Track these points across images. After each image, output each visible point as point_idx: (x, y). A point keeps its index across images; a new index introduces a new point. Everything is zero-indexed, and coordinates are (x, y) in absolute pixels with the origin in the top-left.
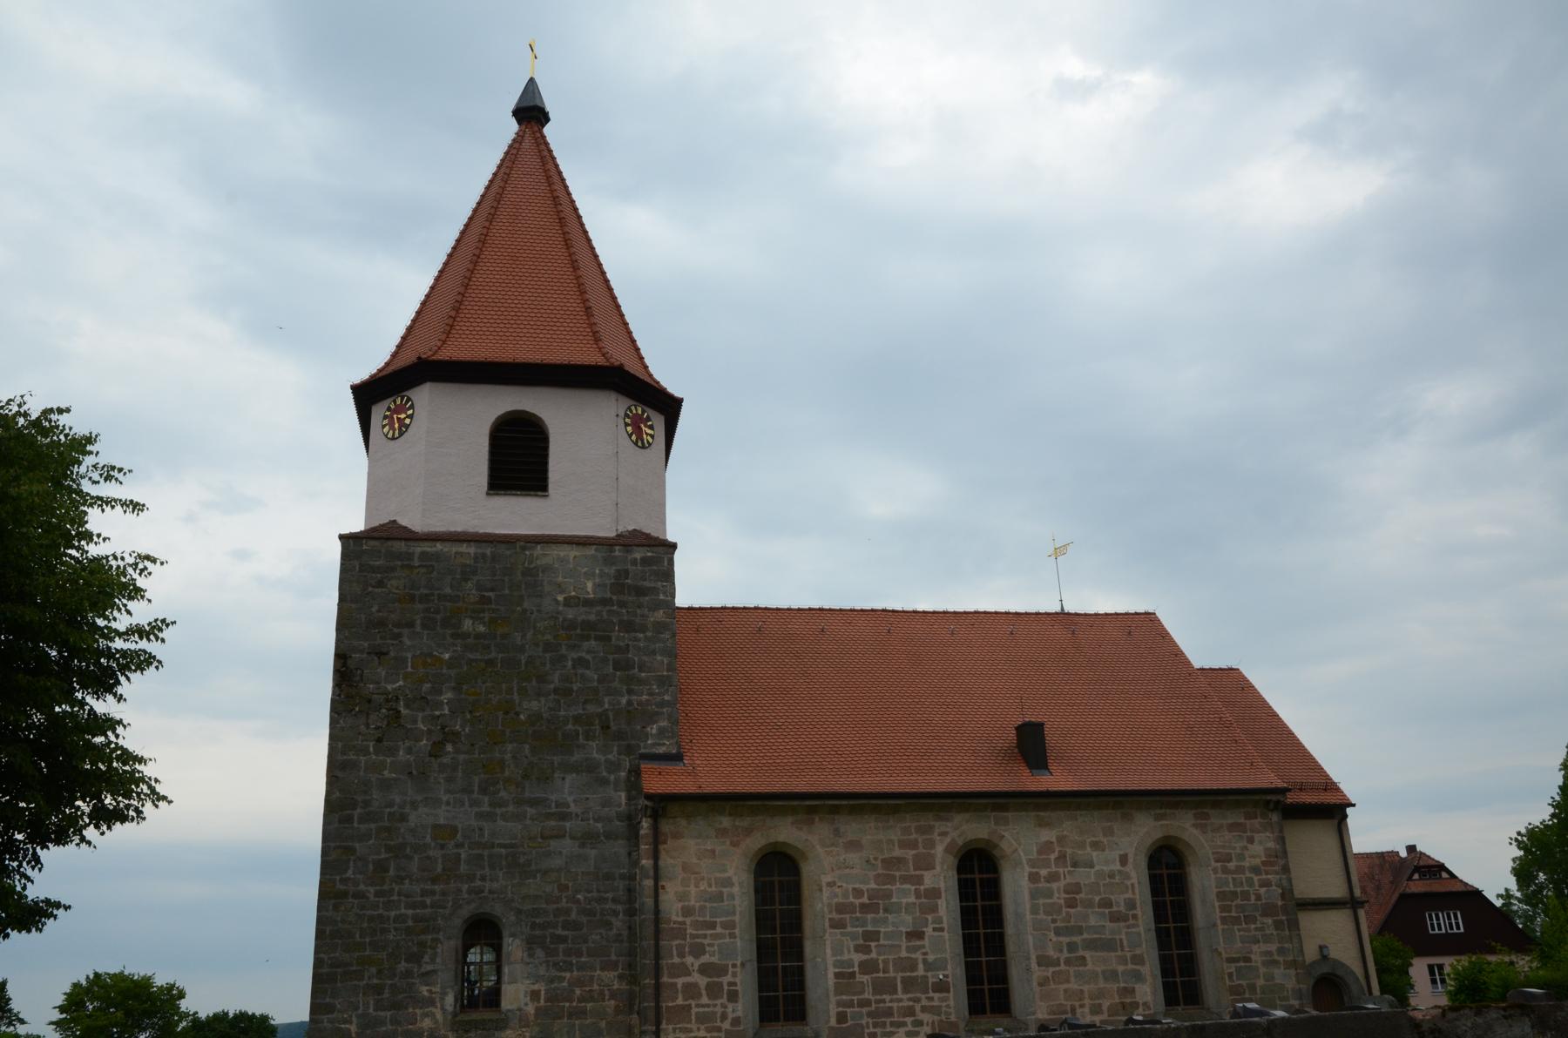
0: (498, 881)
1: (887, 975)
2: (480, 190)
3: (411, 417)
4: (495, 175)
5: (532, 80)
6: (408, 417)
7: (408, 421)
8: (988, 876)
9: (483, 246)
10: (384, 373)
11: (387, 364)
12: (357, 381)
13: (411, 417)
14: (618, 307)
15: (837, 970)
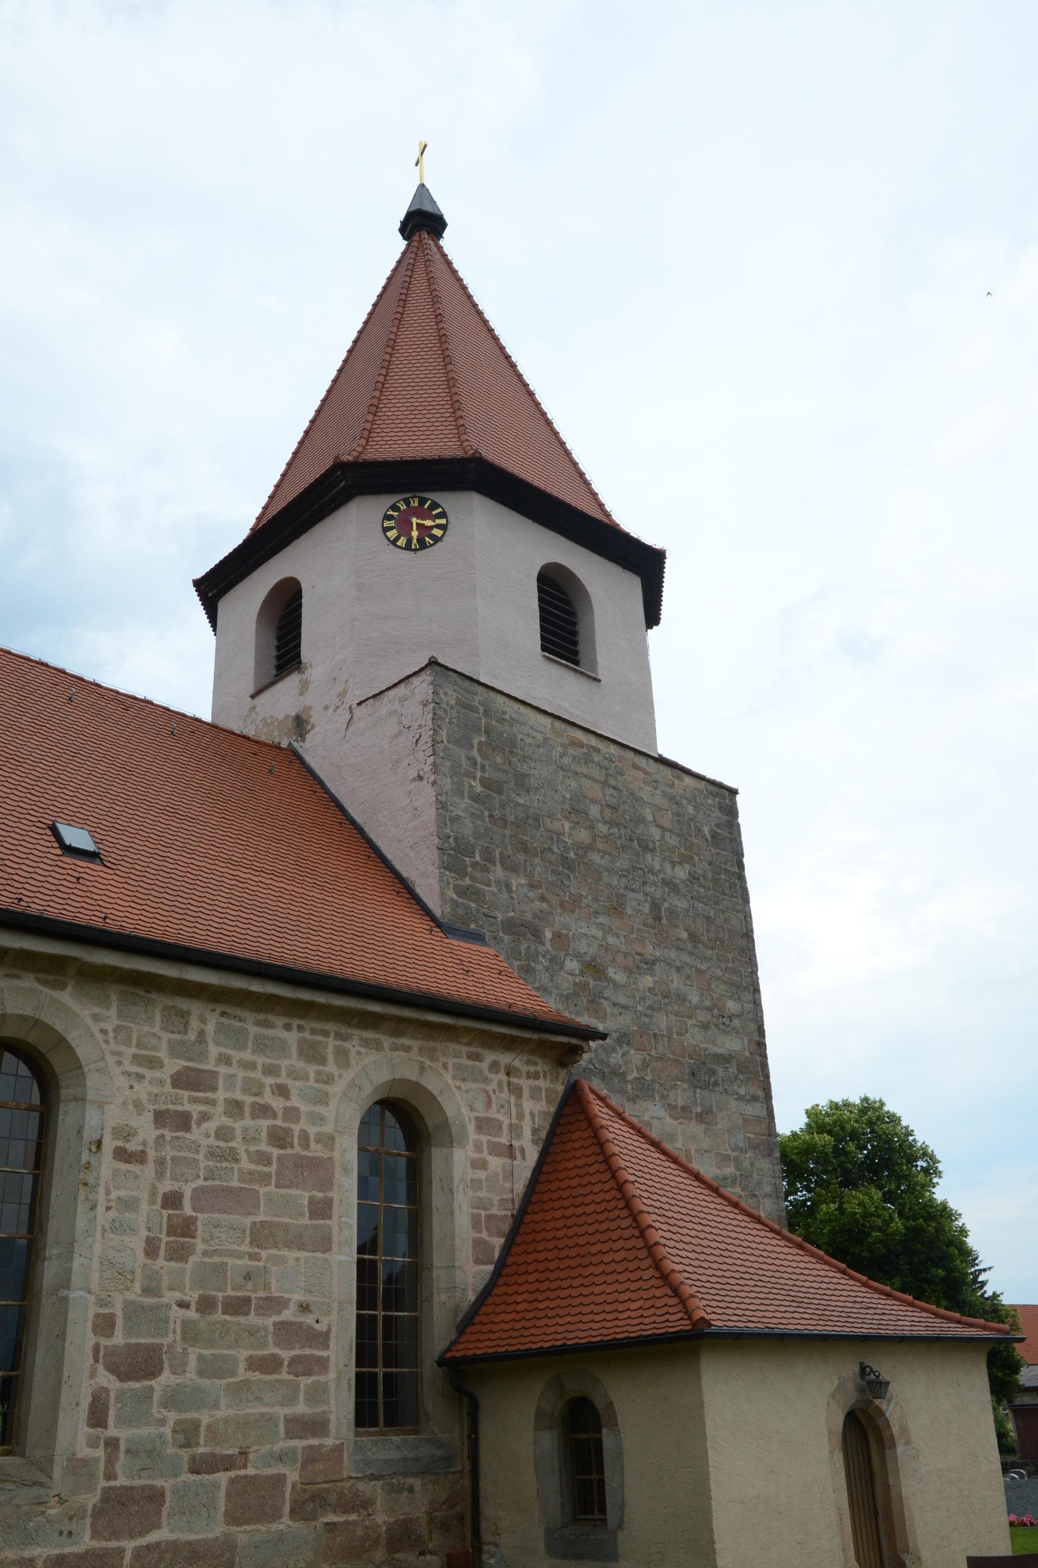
0: (292, 1147)
1: (112, 1483)
2: (523, 475)
3: (443, 527)
4: (399, 262)
5: (422, 186)
6: (439, 526)
7: (438, 532)
8: (397, 1370)
9: (400, 324)
10: (264, 521)
11: (265, 508)
12: (200, 573)
13: (443, 527)
14: (464, 288)
15: (327, 1222)
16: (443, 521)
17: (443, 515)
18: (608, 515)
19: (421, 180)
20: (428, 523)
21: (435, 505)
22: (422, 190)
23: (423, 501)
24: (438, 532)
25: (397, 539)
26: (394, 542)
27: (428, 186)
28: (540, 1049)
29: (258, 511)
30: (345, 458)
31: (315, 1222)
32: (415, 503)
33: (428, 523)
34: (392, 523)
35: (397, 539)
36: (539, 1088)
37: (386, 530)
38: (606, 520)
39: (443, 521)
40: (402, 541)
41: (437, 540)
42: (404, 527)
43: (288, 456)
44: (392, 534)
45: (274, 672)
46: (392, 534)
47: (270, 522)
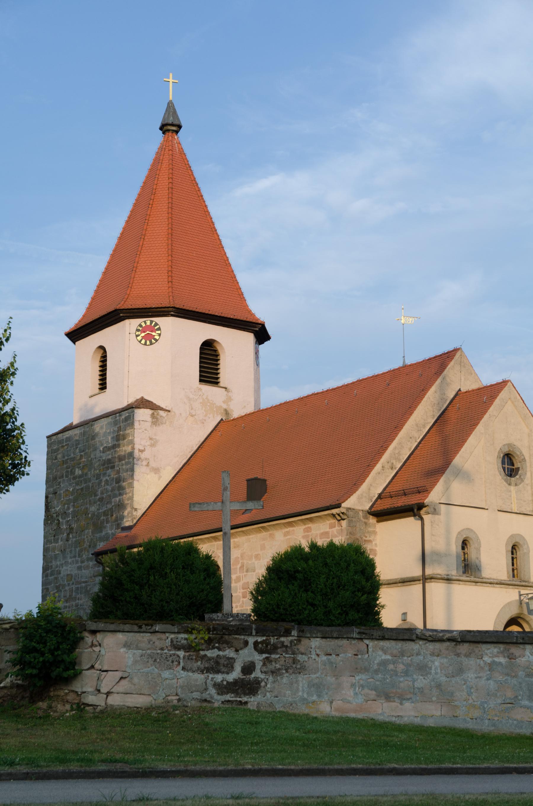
13: (160, 335)
17: (159, 329)
26: (140, 342)
32: (148, 323)
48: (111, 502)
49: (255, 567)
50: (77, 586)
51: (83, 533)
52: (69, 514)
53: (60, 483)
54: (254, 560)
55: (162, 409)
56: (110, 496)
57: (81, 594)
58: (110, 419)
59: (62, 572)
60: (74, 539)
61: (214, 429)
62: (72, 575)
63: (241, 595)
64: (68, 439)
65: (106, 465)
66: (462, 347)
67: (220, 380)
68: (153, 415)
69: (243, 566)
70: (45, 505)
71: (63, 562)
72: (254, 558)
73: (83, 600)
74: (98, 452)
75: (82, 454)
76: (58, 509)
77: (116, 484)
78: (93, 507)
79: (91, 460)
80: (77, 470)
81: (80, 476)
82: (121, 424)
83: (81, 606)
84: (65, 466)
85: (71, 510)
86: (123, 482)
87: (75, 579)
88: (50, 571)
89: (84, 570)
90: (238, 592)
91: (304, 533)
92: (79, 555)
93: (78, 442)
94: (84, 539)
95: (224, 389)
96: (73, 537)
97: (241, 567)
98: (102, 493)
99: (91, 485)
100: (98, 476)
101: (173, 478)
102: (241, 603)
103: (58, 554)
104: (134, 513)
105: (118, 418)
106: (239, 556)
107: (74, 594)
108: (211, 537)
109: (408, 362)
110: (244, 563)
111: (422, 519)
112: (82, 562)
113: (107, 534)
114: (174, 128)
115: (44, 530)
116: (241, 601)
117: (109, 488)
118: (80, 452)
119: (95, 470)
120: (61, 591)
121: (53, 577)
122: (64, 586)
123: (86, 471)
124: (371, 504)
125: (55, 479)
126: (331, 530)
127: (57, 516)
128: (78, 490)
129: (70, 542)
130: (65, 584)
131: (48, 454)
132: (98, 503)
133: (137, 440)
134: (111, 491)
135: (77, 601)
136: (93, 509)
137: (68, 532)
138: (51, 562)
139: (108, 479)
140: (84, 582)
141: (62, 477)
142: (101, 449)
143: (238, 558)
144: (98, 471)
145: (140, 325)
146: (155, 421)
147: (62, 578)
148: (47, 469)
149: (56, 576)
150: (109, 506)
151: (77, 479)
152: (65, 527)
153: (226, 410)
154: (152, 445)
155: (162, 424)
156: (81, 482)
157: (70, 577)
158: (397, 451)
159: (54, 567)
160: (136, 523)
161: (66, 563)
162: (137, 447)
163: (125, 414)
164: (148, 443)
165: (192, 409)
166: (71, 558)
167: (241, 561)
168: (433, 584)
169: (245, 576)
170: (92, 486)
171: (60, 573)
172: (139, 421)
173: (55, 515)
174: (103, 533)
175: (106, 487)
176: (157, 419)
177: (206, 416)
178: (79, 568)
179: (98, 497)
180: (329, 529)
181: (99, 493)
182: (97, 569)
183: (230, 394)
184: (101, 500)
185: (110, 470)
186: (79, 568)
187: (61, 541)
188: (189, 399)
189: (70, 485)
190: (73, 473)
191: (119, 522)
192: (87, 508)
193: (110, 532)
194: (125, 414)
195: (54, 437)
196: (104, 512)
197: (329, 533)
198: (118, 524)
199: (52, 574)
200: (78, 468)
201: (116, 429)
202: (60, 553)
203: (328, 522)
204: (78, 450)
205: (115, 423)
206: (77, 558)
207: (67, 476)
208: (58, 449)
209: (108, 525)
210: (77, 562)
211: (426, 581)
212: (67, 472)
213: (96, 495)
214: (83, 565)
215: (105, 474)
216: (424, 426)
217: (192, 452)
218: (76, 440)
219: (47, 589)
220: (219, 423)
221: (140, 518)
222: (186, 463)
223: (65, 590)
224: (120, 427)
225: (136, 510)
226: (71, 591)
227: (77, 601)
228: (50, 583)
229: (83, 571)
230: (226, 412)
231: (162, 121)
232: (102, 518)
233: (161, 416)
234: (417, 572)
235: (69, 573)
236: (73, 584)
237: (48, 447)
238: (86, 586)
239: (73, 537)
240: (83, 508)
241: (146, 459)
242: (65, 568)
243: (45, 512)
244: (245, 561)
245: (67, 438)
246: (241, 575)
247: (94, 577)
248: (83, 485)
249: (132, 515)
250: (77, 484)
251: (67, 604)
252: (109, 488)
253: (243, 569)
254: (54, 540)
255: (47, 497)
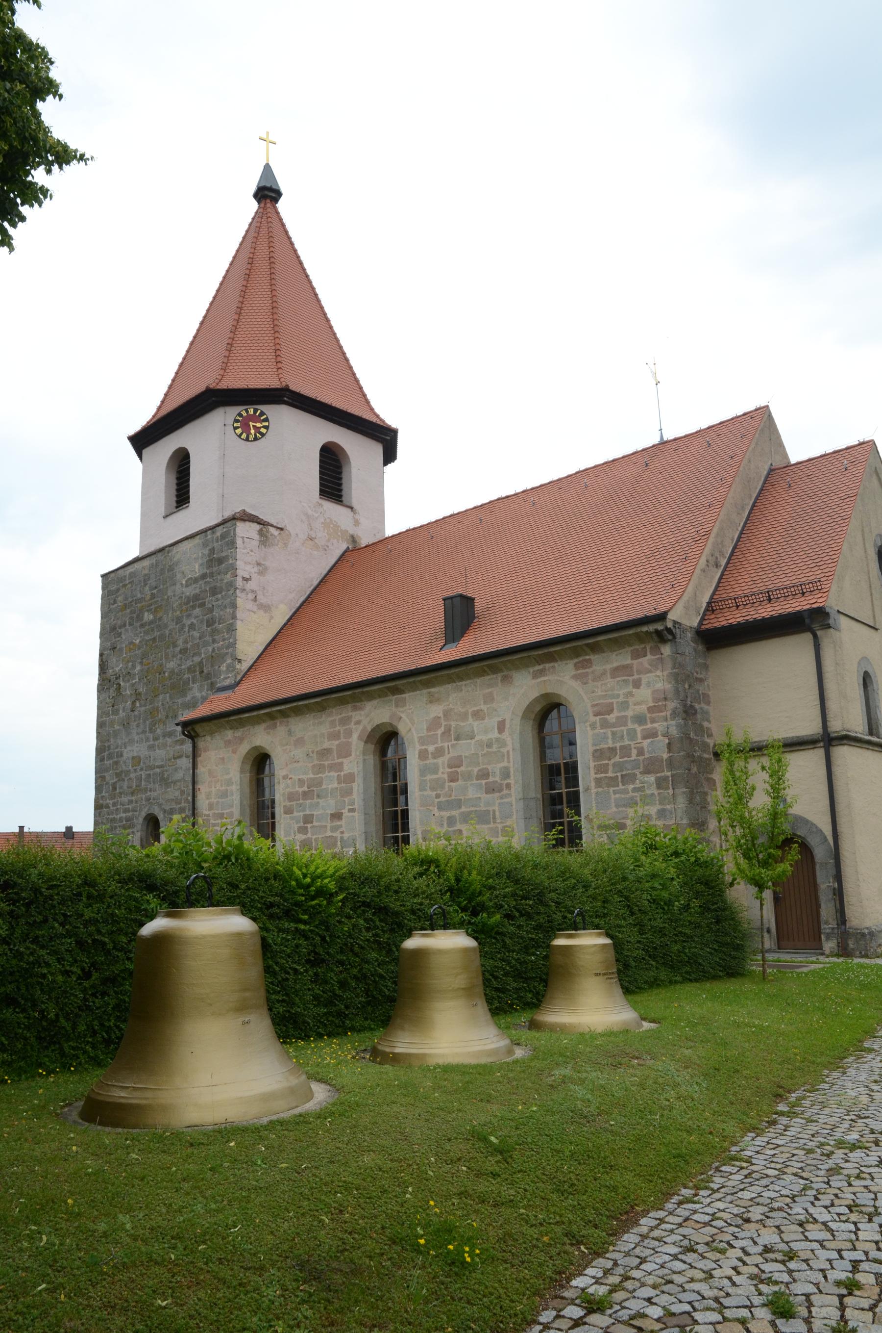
3: (267, 427)
6: (264, 427)
7: (263, 430)
11: (154, 416)
13: (267, 427)
16: (266, 424)
17: (267, 420)
18: (383, 421)
19: (268, 160)
20: (258, 425)
21: (262, 414)
22: (267, 169)
23: (256, 410)
24: (263, 430)
25: (242, 434)
26: (240, 436)
27: (271, 165)
28: (641, 638)
29: (151, 417)
30: (211, 387)
31: (579, 672)
32: (251, 411)
33: (258, 425)
34: (238, 425)
35: (242, 434)
36: (637, 650)
37: (235, 428)
38: (379, 422)
39: (266, 424)
40: (244, 436)
41: (263, 435)
42: (246, 427)
43: (362, 383)
44: (239, 431)
45: (175, 504)
46: (239, 431)
47: (154, 423)
48: (200, 654)
49: (473, 732)
50: (148, 772)
51: (156, 699)
52: (135, 675)
53: (121, 633)
54: (470, 719)
55: (272, 526)
56: (198, 645)
57: (154, 783)
58: (197, 540)
59: (125, 755)
60: (143, 708)
61: (339, 560)
62: (139, 758)
63: (446, 776)
64: (132, 575)
65: (191, 604)
66: (770, 404)
67: (344, 499)
68: (260, 532)
69: (450, 730)
70: (100, 665)
71: (127, 740)
72: (470, 717)
73: (158, 792)
74: (178, 586)
75: (155, 591)
76: (117, 669)
77: (207, 626)
78: (172, 663)
79: (168, 598)
80: (146, 614)
81: (151, 622)
82: (215, 545)
83: (154, 799)
84: (128, 611)
85: (138, 668)
86: (219, 624)
87: (144, 763)
88: (107, 753)
89: (159, 749)
90: (440, 773)
91: (577, 670)
92: (151, 729)
93: (147, 578)
94: (158, 707)
95: (349, 510)
96: (141, 706)
97: (443, 733)
98: (186, 642)
99: (167, 632)
100: (179, 620)
101: (289, 620)
102: (447, 789)
103: (119, 730)
104: (238, 667)
105: (209, 537)
106: (441, 715)
107: (143, 783)
108: (387, 688)
109: (668, 436)
110: (450, 726)
111: (815, 637)
112: (155, 739)
113: (194, 697)
114: (273, 195)
115: (98, 698)
116: (446, 787)
117: (196, 634)
118: (151, 589)
119: (174, 611)
120: (124, 780)
121: (111, 761)
122: (128, 772)
123: (159, 616)
124: (699, 618)
125: (113, 629)
126: (635, 662)
127: (117, 679)
128: (147, 641)
129: (136, 713)
130: (129, 771)
131: (102, 598)
132: (180, 656)
133: (240, 564)
134: (200, 638)
135: (149, 793)
136: (171, 665)
137: (133, 699)
138: (108, 740)
139: (195, 621)
140: (158, 767)
141: (125, 625)
142: (184, 582)
143: (439, 718)
144: (178, 613)
145: (240, 415)
146: (264, 539)
147: (125, 762)
148: (102, 618)
149: (115, 760)
150: (197, 659)
151: (147, 627)
152: (128, 692)
153: (352, 537)
154: (261, 573)
155: (273, 545)
156: (153, 630)
157: (137, 760)
158: (719, 540)
159: (112, 747)
160: (241, 680)
161: (131, 741)
162: (241, 573)
163: (219, 531)
164: (256, 569)
165: (311, 529)
166: (138, 734)
167: (444, 723)
168: (845, 748)
169: (453, 746)
170: (170, 634)
171: (122, 756)
172: (243, 538)
173: (113, 678)
174: (188, 698)
175: (191, 633)
176: (267, 537)
177: (328, 540)
178: (151, 748)
179: (178, 649)
180: (632, 659)
181: (180, 642)
182: (178, 747)
183: (357, 517)
184: (184, 651)
185: (198, 609)
186: (151, 748)
187: (124, 711)
188: (308, 517)
189: (136, 635)
190: (139, 618)
191: (213, 680)
192: (161, 665)
193: (198, 695)
194: (219, 531)
195: (113, 575)
196: (189, 669)
197: (631, 667)
198: (212, 683)
199: (110, 757)
200: (148, 611)
201: (206, 552)
202: (121, 728)
203: (531, 670)
204: (147, 588)
205: (205, 545)
206: (148, 734)
207: (130, 624)
208: (118, 590)
209: (195, 685)
210: (147, 740)
211: (834, 743)
212: (131, 618)
213: (175, 646)
214: (156, 743)
215: (189, 616)
216: (743, 508)
217: (312, 588)
218: (146, 575)
219: (103, 778)
220: (345, 552)
221: (246, 673)
222: (304, 602)
223: (130, 779)
224: (213, 548)
225: (240, 661)
226: (139, 779)
227: (149, 793)
228: (107, 770)
229: (157, 751)
230: (353, 540)
231: (259, 183)
232: (186, 676)
233: (272, 535)
234: (810, 727)
235: (135, 754)
236: (142, 769)
237: (103, 588)
238: (162, 773)
239: (141, 706)
240: (156, 664)
241: (253, 591)
242: (129, 748)
243: (100, 674)
244: (453, 724)
245: (131, 574)
246: (446, 745)
247: (174, 758)
248: (157, 634)
249: (234, 669)
250: (146, 633)
251: (133, 798)
252: (196, 634)
253: (450, 735)
254: (112, 711)
255: (101, 655)
